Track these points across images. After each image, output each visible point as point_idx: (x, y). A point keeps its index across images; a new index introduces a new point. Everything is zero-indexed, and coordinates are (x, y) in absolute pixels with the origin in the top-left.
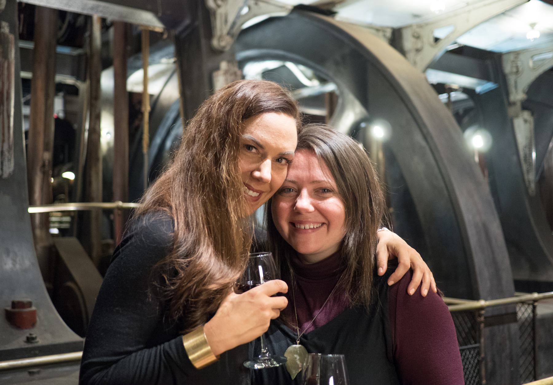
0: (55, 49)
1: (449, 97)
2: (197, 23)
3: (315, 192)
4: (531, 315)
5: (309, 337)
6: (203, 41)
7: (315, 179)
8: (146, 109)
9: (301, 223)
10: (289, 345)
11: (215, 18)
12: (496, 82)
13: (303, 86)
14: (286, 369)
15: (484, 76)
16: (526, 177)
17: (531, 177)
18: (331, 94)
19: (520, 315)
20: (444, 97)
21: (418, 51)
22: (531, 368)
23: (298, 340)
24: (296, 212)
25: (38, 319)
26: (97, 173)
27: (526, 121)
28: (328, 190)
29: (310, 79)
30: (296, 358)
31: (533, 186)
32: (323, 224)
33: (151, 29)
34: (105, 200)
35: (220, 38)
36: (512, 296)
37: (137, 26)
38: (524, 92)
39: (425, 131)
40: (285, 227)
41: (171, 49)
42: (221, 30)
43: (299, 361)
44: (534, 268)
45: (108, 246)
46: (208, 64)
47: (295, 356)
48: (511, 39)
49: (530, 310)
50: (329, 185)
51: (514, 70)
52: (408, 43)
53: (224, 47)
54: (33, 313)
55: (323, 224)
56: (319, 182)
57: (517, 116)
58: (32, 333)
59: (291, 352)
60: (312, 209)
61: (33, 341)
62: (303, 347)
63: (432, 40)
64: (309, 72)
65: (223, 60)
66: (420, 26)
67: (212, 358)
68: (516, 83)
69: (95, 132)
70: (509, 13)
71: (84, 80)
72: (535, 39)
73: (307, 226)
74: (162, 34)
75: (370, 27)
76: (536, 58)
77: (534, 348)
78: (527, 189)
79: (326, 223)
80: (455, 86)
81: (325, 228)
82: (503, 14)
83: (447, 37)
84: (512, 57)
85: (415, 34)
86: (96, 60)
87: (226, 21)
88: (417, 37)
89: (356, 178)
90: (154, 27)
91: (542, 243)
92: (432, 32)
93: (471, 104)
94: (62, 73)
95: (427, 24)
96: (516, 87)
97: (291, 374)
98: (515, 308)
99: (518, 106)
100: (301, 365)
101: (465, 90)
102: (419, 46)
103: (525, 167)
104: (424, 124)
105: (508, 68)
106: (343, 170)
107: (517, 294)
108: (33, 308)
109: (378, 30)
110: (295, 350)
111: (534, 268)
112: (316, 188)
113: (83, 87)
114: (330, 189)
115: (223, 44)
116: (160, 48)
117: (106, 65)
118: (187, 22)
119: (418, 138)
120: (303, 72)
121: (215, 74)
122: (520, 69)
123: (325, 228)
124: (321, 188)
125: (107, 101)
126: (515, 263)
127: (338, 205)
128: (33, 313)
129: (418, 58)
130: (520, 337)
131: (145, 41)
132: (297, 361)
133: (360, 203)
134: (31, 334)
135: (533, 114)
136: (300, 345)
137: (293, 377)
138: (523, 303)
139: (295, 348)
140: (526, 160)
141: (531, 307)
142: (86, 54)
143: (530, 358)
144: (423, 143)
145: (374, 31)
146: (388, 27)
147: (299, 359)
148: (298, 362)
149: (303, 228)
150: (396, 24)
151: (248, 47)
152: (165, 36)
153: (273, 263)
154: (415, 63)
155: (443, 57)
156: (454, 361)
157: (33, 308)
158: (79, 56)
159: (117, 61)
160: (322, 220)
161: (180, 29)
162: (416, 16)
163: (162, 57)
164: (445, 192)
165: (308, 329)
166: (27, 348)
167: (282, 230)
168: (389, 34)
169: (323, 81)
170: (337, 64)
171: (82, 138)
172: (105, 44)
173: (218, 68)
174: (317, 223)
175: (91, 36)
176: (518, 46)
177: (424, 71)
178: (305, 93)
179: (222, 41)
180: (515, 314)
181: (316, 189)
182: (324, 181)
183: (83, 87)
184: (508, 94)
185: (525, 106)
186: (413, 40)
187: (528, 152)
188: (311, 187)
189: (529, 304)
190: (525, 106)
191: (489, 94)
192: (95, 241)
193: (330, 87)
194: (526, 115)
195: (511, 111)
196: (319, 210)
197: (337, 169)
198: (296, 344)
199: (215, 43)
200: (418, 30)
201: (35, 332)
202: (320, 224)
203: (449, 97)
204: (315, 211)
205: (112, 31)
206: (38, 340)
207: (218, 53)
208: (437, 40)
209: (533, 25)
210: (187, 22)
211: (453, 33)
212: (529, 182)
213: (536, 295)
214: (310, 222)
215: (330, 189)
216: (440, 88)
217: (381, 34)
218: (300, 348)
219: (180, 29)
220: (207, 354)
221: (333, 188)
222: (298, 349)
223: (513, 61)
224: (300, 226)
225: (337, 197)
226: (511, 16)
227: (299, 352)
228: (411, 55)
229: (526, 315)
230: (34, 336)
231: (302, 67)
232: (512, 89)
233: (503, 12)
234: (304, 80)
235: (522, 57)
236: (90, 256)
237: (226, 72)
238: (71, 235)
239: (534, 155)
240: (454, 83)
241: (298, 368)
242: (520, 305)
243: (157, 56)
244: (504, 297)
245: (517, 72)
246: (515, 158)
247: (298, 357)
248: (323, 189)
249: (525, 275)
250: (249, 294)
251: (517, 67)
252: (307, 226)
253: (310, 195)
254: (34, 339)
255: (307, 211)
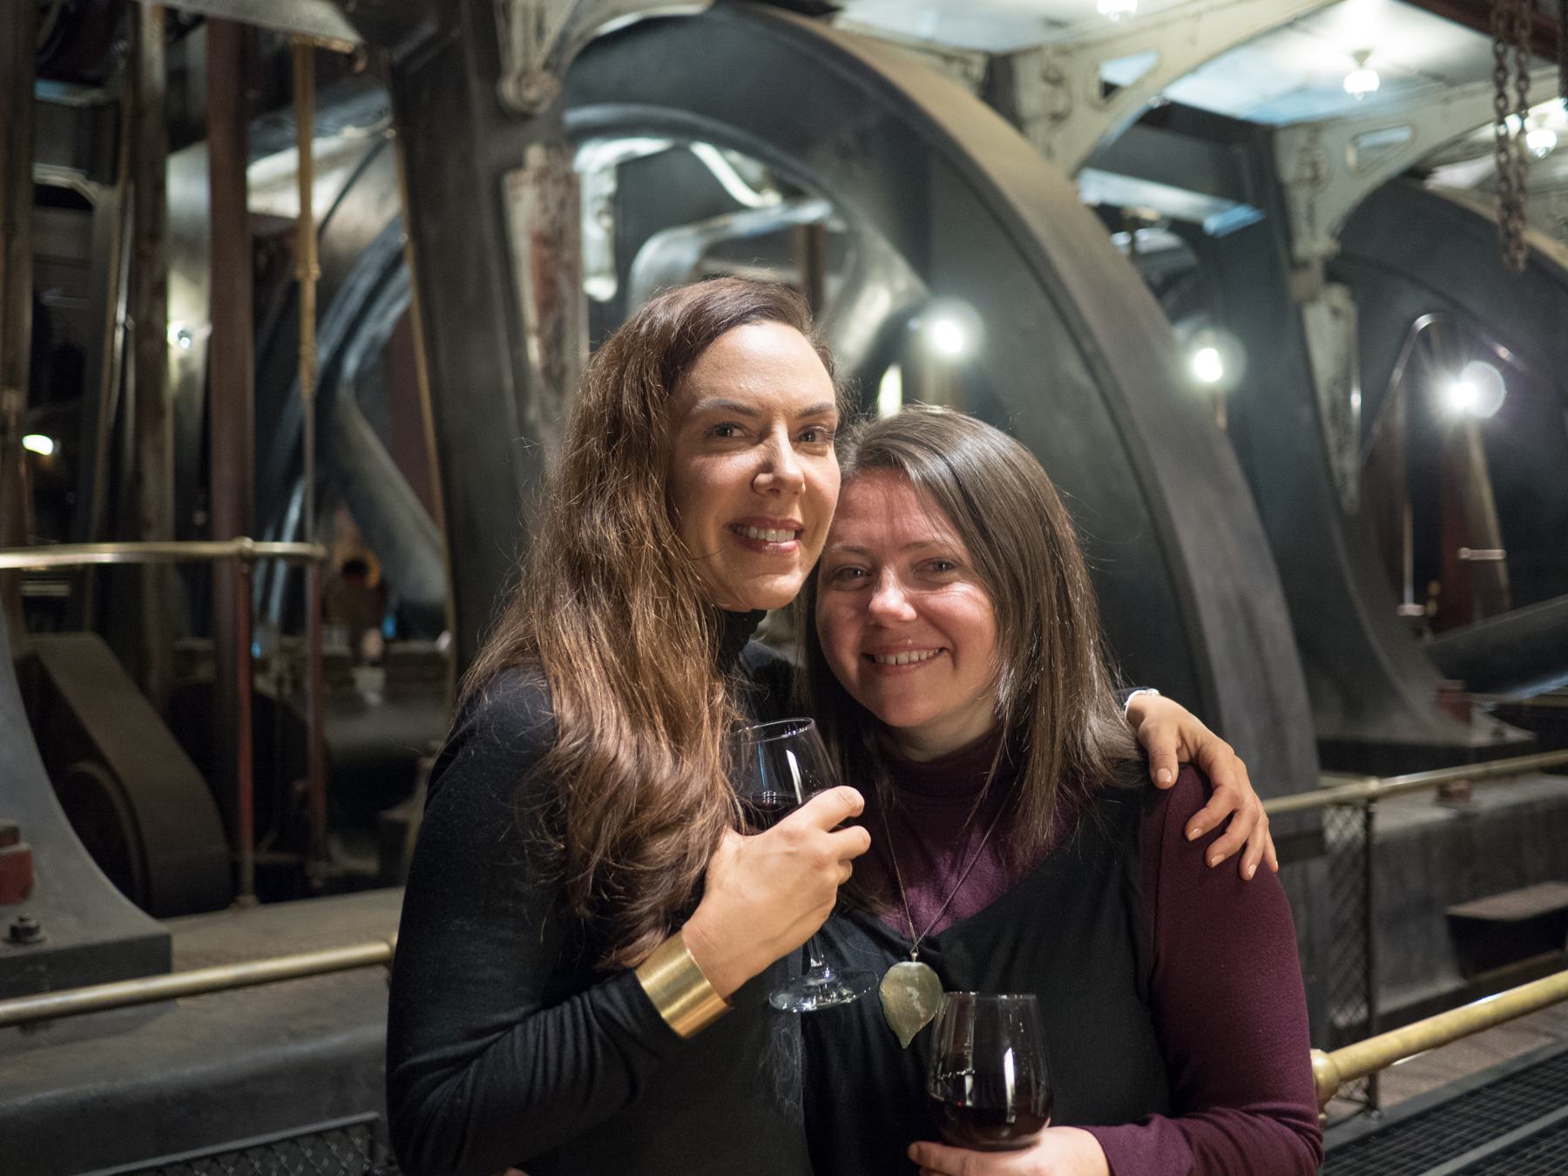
0: (32, 89)
1: (1133, 242)
2: (455, 33)
3: (917, 571)
4: (1361, 836)
5: (943, 945)
6: (475, 86)
7: (914, 539)
8: (308, 274)
9: (888, 650)
10: (889, 965)
11: (508, 21)
12: (1257, 204)
13: (738, 207)
14: (889, 1027)
15: (1228, 189)
16: (1335, 463)
17: (1348, 463)
18: (813, 231)
19: (1331, 835)
20: (1121, 239)
21: (1058, 118)
22: (1357, 975)
23: (915, 951)
24: (875, 626)
25: (36, 876)
26: (160, 450)
27: (1336, 313)
28: (947, 564)
29: (756, 188)
30: (911, 995)
31: (1352, 487)
32: (941, 650)
33: (320, 43)
34: (184, 532)
35: (524, 77)
36: (1314, 787)
37: (271, 34)
38: (1333, 235)
39: (1088, 347)
40: (851, 664)
41: (380, 99)
42: (526, 54)
43: (918, 1003)
44: (1354, 707)
45: (190, 656)
46: (490, 150)
47: (909, 989)
48: (1302, 90)
49: (1356, 825)
50: (948, 552)
51: (1308, 173)
52: (1032, 96)
53: (535, 104)
54: (24, 860)
55: (941, 650)
56: (921, 545)
57: (1313, 298)
58: (26, 915)
59: (897, 980)
60: (909, 612)
61: (29, 939)
62: (927, 968)
63: (1095, 91)
64: (754, 169)
65: (532, 140)
66: (1064, 51)
67: (715, 1005)
68: (1311, 207)
69: (149, 332)
70: (1303, 24)
71: (112, 181)
72: (1367, 94)
73: (903, 657)
74: (351, 58)
75: (927, 48)
76: (1366, 141)
77: (1366, 924)
78: (1336, 494)
79: (947, 647)
80: (1148, 214)
81: (944, 660)
82: (1291, 24)
83: (1138, 83)
84: (1301, 138)
85: (1051, 74)
86: (152, 124)
87: (540, 31)
88: (1056, 80)
89: (1017, 529)
90: (331, 39)
91: (1374, 641)
92: (1097, 69)
93: (1189, 258)
94: (48, 159)
95: (1083, 46)
96: (1311, 220)
97: (898, 1034)
98: (1319, 820)
99: (1316, 273)
100: (924, 1013)
101: (1176, 225)
102: (1060, 105)
103: (1332, 436)
104: (1088, 332)
105: (1290, 167)
106: (979, 513)
107: (1326, 780)
108: (23, 846)
109: (948, 58)
110: (909, 975)
111: (1354, 707)
112: (918, 560)
113: (104, 197)
114: (952, 560)
115: (532, 94)
116: (341, 99)
117: (182, 136)
118: (428, 29)
119: (1072, 366)
120: (735, 168)
121: (509, 179)
122: (1323, 171)
123: (944, 660)
124: (928, 561)
125: (188, 245)
126: (1315, 701)
127: (976, 600)
128: (24, 860)
129: (1058, 139)
130: (1333, 894)
131: (303, 75)
132: (915, 1004)
133: (1029, 593)
134: (22, 920)
135: (1353, 297)
136: (920, 964)
137: (906, 1042)
138: (1340, 804)
139: (907, 968)
140: (1334, 418)
141: (1361, 815)
142: (116, 104)
143: (1356, 950)
144: (1084, 380)
145: (936, 61)
146: (975, 52)
147: (918, 999)
148: (918, 1006)
149: (894, 662)
150: (1000, 42)
151: (587, 97)
152: (360, 65)
153: (822, 752)
154: (1049, 152)
155: (1126, 136)
156: (1290, 997)
157: (23, 846)
158: (95, 108)
159: (219, 131)
160: (936, 640)
161: (406, 47)
162: (1054, 24)
163: (344, 122)
164: (1143, 512)
165: (936, 923)
166: (14, 958)
167: (843, 670)
168: (978, 70)
169: (793, 194)
170: (844, 154)
171: (107, 347)
172: (177, 76)
173: (518, 164)
174: (928, 649)
175: (135, 57)
176: (1320, 108)
177: (1075, 175)
178: (741, 225)
179: (528, 85)
180: (1319, 834)
181: (918, 564)
182: (935, 541)
183: (104, 197)
184: (1289, 237)
185: (1335, 272)
186: (1045, 88)
187: (1341, 397)
188: (904, 560)
189: (1355, 809)
190: (1335, 272)
191: (1240, 235)
192: (154, 642)
193: (813, 211)
194: (1337, 296)
195: (1299, 284)
196: (931, 619)
197: (966, 511)
198: (910, 959)
199: (509, 89)
200: (1059, 61)
201: (31, 912)
202: (937, 651)
203: (1133, 242)
204: (918, 617)
205: (198, 40)
206: (42, 934)
207: (515, 118)
208: (1109, 89)
209: (1361, 57)
210: (428, 29)
211: (1152, 72)
212: (1344, 476)
213: (1373, 785)
214: (910, 649)
215: (952, 562)
216: (1113, 217)
217: (956, 68)
218: (920, 969)
219: (406, 47)
220: (705, 996)
221: (960, 559)
222: (916, 974)
223: (1304, 150)
224: (885, 659)
225: (973, 581)
226: (1306, 31)
227: (917, 979)
228: (1039, 129)
229: (1347, 834)
230: (32, 923)
231: (735, 157)
232: (1301, 225)
233: (1290, 20)
234: (740, 191)
235: (1327, 138)
236: (142, 685)
237: (542, 176)
238: (77, 628)
239: (1356, 400)
240: (1147, 206)
241: (918, 1020)
242: (1331, 812)
243: (330, 121)
244: (1292, 792)
245: (1315, 180)
246: (1306, 412)
247: (916, 994)
248: (934, 563)
249: (1334, 727)
250: (781, 833)
251: (1314, 165)
252: (903, 657)
253: (904, 580)
254: (31, 931)
255: (896, 617)
